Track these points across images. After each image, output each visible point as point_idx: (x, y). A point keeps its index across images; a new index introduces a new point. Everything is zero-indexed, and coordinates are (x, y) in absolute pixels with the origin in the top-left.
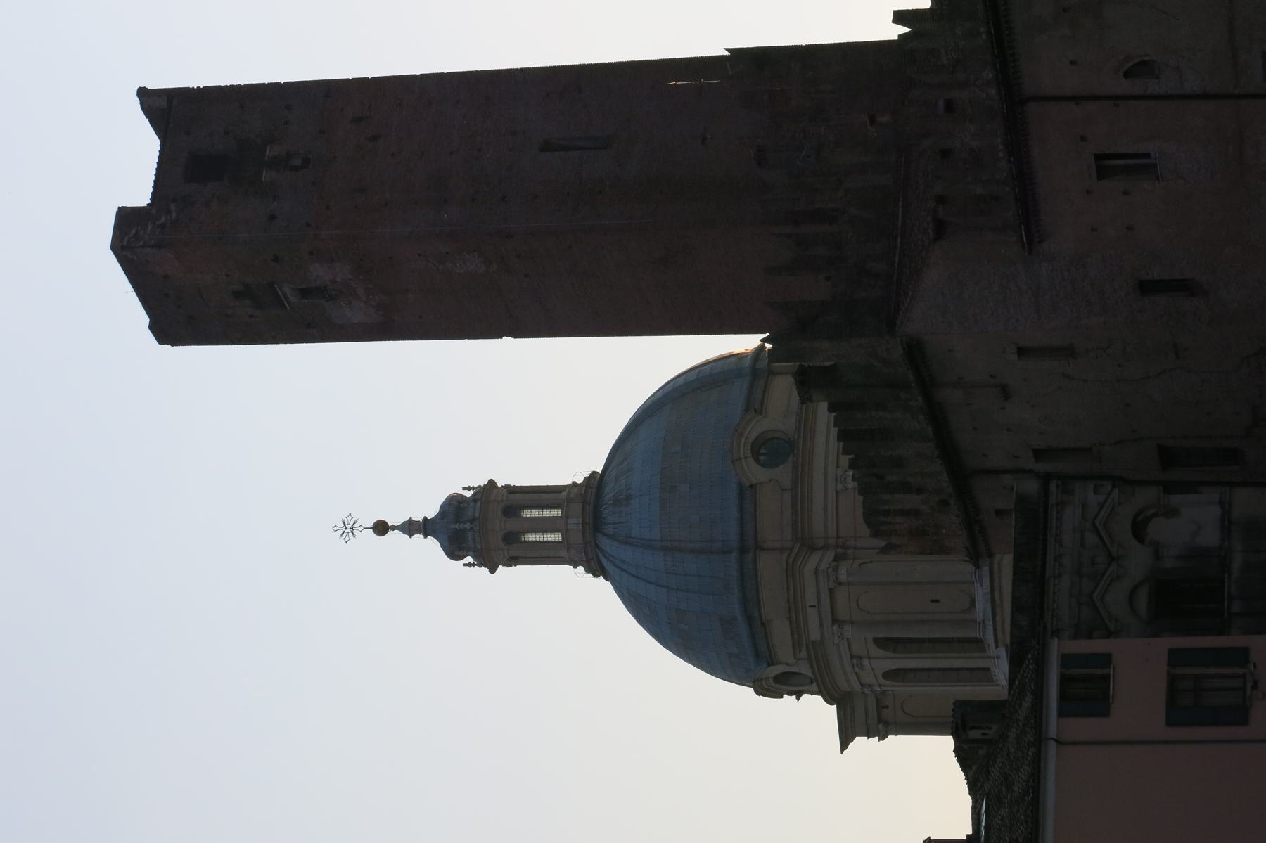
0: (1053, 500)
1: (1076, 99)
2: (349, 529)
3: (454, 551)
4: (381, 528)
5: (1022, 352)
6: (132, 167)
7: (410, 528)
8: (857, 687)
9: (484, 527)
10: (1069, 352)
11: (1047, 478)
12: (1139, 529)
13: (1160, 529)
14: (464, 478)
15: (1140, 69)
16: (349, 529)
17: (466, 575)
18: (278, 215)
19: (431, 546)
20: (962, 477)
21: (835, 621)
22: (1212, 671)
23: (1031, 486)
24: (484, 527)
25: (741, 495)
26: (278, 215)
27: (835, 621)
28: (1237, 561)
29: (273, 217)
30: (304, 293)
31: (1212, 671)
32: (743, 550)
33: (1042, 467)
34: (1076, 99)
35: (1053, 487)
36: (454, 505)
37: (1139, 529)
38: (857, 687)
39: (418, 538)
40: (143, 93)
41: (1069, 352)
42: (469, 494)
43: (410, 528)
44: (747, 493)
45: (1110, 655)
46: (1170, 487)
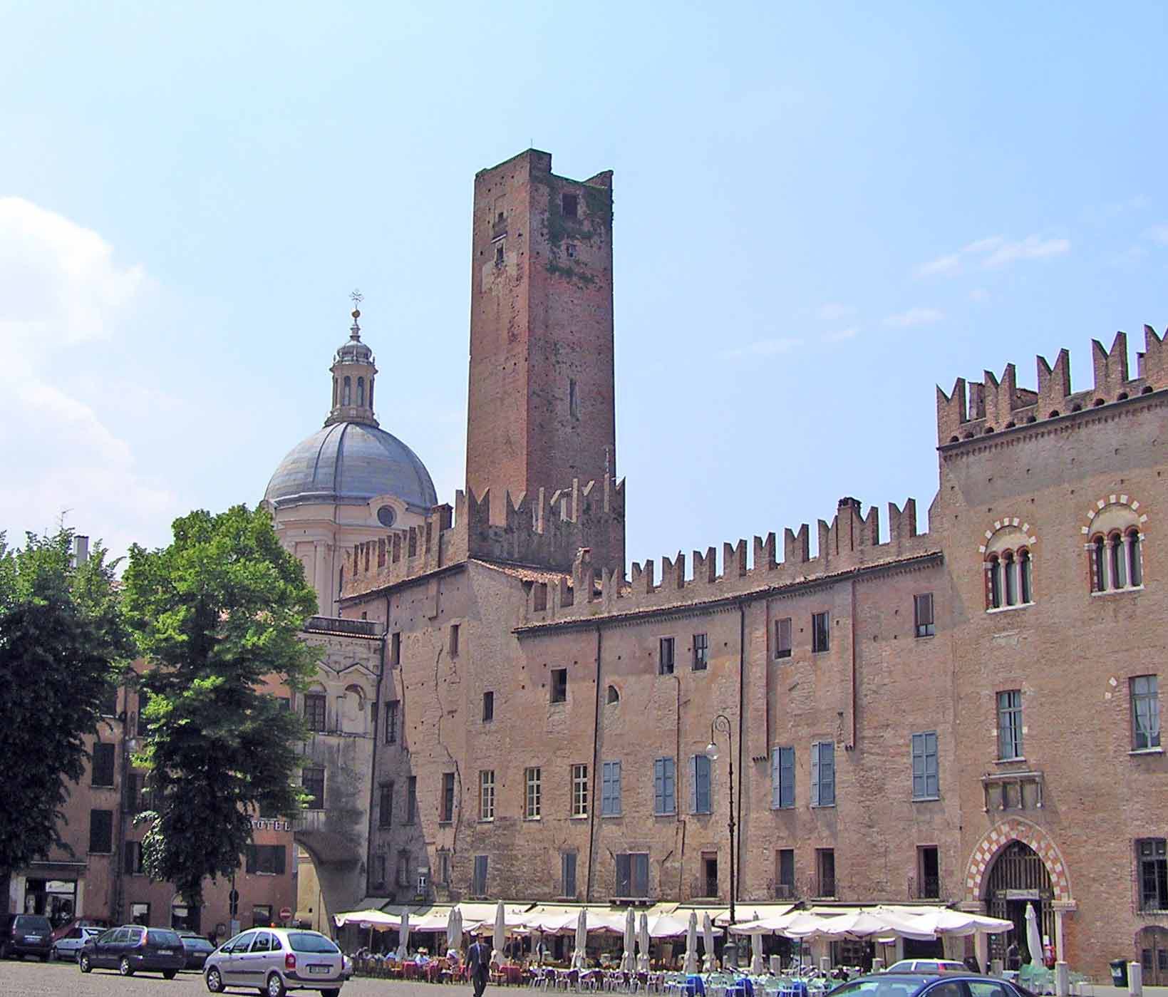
1: (599, 660)
2: (357, 297)
3: (344, 352)
4: (356, 314)
5: (456, 628)
6: (572, 166)
9: (354, 375)
10: (454, 652)
11: (383, 640)
12: (353, 688)
13: (353, 698)
14: (379, 358)
15: (614, 696)
17: (329, 358)
18: (548, 234)
19: (345, 340)
20: (387, 594)
21: (297, 544)
22: (574, 504)
23: (378, 630)
24: (354, 375)
25: (365, 499)
26: (548, 234)
27: (297, 544)
28: (333, 741)
30: (500, 251)
31: (574, 504)
32: (335, 498)
33: (389, 637)
34: (599, 660)
36: (366, 353)
37: (353, 688)
40: (611, 172)
41: (454, 652)
44: (365, 501)
46: (375, 706)
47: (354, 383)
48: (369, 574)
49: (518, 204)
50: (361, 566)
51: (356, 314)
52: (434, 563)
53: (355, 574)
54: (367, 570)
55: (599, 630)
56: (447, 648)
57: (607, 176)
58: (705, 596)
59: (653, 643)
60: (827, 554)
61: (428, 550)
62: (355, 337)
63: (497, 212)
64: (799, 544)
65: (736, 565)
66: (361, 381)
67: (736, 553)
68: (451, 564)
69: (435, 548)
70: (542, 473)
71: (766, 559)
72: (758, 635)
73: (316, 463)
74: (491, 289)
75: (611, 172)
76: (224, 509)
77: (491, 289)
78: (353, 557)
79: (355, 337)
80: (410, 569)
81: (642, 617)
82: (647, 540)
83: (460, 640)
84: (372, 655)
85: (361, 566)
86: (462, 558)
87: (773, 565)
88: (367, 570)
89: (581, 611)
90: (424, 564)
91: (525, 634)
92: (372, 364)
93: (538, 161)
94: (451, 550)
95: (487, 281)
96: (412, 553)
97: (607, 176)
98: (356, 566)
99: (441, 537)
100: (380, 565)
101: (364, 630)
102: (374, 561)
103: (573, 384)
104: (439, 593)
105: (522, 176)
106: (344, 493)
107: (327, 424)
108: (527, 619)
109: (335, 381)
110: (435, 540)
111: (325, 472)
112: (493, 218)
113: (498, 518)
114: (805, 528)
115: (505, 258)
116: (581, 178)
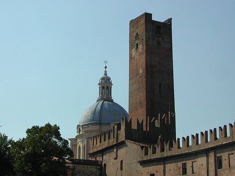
0: (97, 167)
2: (106, 62)
3: (103, 79)
4: (106, 67)
6: (159, 17)
7: (106, 72)
8: (78, 141)
9: (106, 85)
10: (121, 169)
14: (113, 80)
16: (106, 62)
17: (98, 81)
18: (154, 39)
19: (102, 75)
21: (88, 138)
24: (106, 85)
26: (154, 39)
29: (150, 39)
30: (137, 45)
35: (99, 167)
36: (109, 79)
38: (78, 141)
39: (104, 73)
40: (171, 19)
41: (121, 169)
42: (111, 81)
43: (106, 72)
45: (152, 14)
47: (105, 88)
48: (97, 145)
49: (141, 30)
50: (95, 143)
51: (106, 67)
52: (115, 141)
53: (93, 145)
54: (96, 144)
55: (163, 161)
56: (119, 168)
57: (170, 20)
58: (195, 149)
59: (180, 164)
60: (232, 135)
61: (114, 137)
62: (106, 74)
63: (136, 33)
64: (223, 132)
65: (204, 139)
66: (107, 88)
67: (205, 135)
68: (120, 141)
69: (116, 136)
70: (151, 112)
71: (213, 137)
72: (212, 160)
73: (94, 113)
74: (135, 57)
75: (171, 19)
76: (44, 126)
77: (135, 57)
78: (92, 140)
79: (106, 74)
80: (109, 143)
81: (177, 156)
82: (182, 131)
83: (123, 165)
84: (98, 171)
85: (95, 143)
86: (123, 139)
87: (216, 139)
88: (96, 144)
89: (159, 154)
90: (113, 141)
91: (144, 163)
92: (111, 83)
93: (148, 16)
94: (120, 137)
95: (134, 54)
96: (109, 138)
97: (170, 20)
98: (93, 143)
99: (117, 132)
100: (100, 142)
101: (95, 163)
102: (98, 141)
103: (160, 84)
104: (117, 151)
105: (143, 21)
106: (103, 122)
107: (98, 101)
108: (142, 158)
109: (100, 88)
110: (116, 133)
111: (97, 115)
112: (135, 35)
113: (134, 126)
114: (225, 126)
115: (139, 47)
116: (162, 21)
